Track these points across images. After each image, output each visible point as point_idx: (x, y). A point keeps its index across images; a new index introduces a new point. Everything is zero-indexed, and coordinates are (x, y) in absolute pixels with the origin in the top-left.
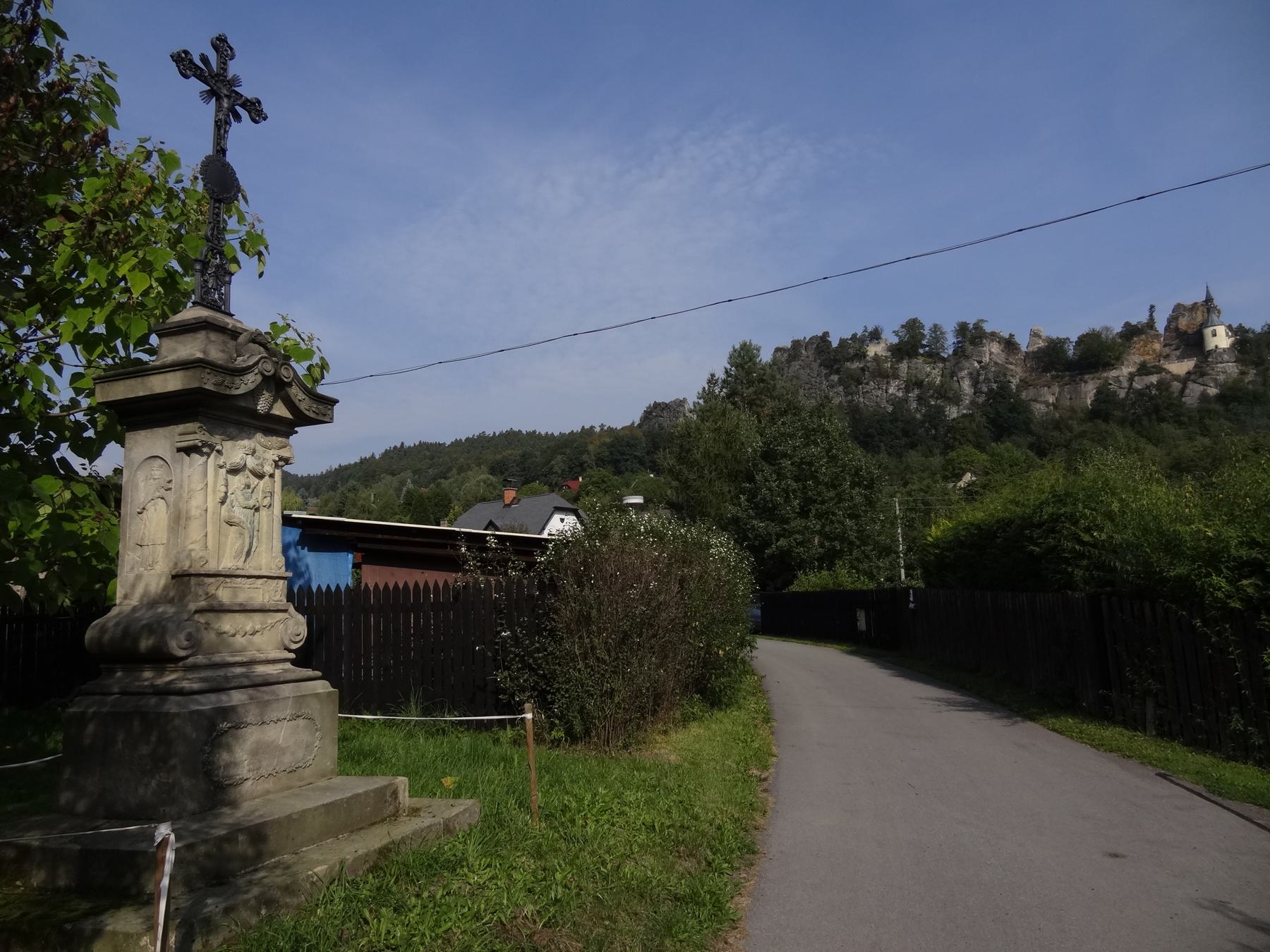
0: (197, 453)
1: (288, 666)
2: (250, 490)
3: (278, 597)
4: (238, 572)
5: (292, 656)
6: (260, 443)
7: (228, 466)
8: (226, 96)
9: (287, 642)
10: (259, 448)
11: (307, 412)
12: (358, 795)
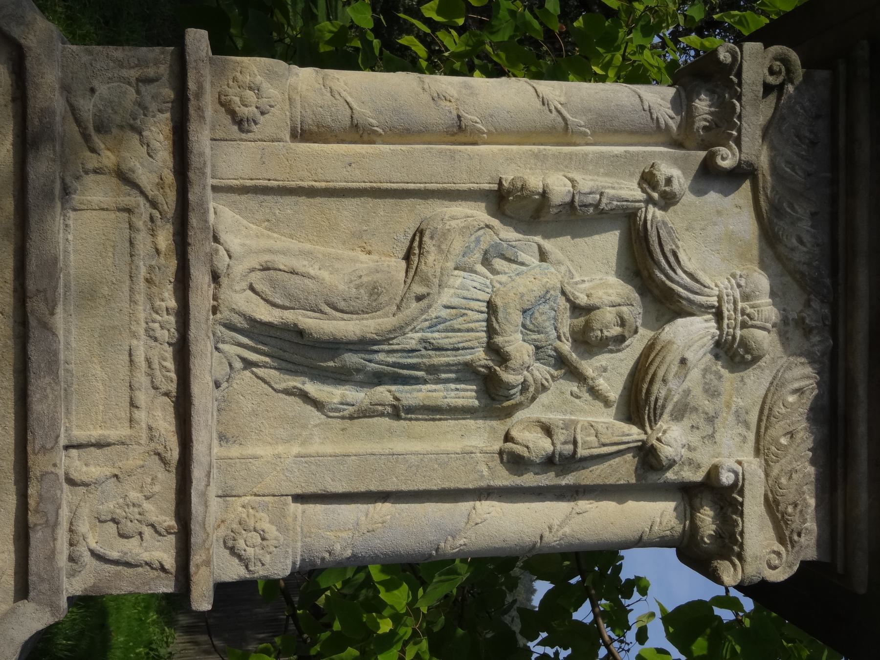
6: (775, 385)
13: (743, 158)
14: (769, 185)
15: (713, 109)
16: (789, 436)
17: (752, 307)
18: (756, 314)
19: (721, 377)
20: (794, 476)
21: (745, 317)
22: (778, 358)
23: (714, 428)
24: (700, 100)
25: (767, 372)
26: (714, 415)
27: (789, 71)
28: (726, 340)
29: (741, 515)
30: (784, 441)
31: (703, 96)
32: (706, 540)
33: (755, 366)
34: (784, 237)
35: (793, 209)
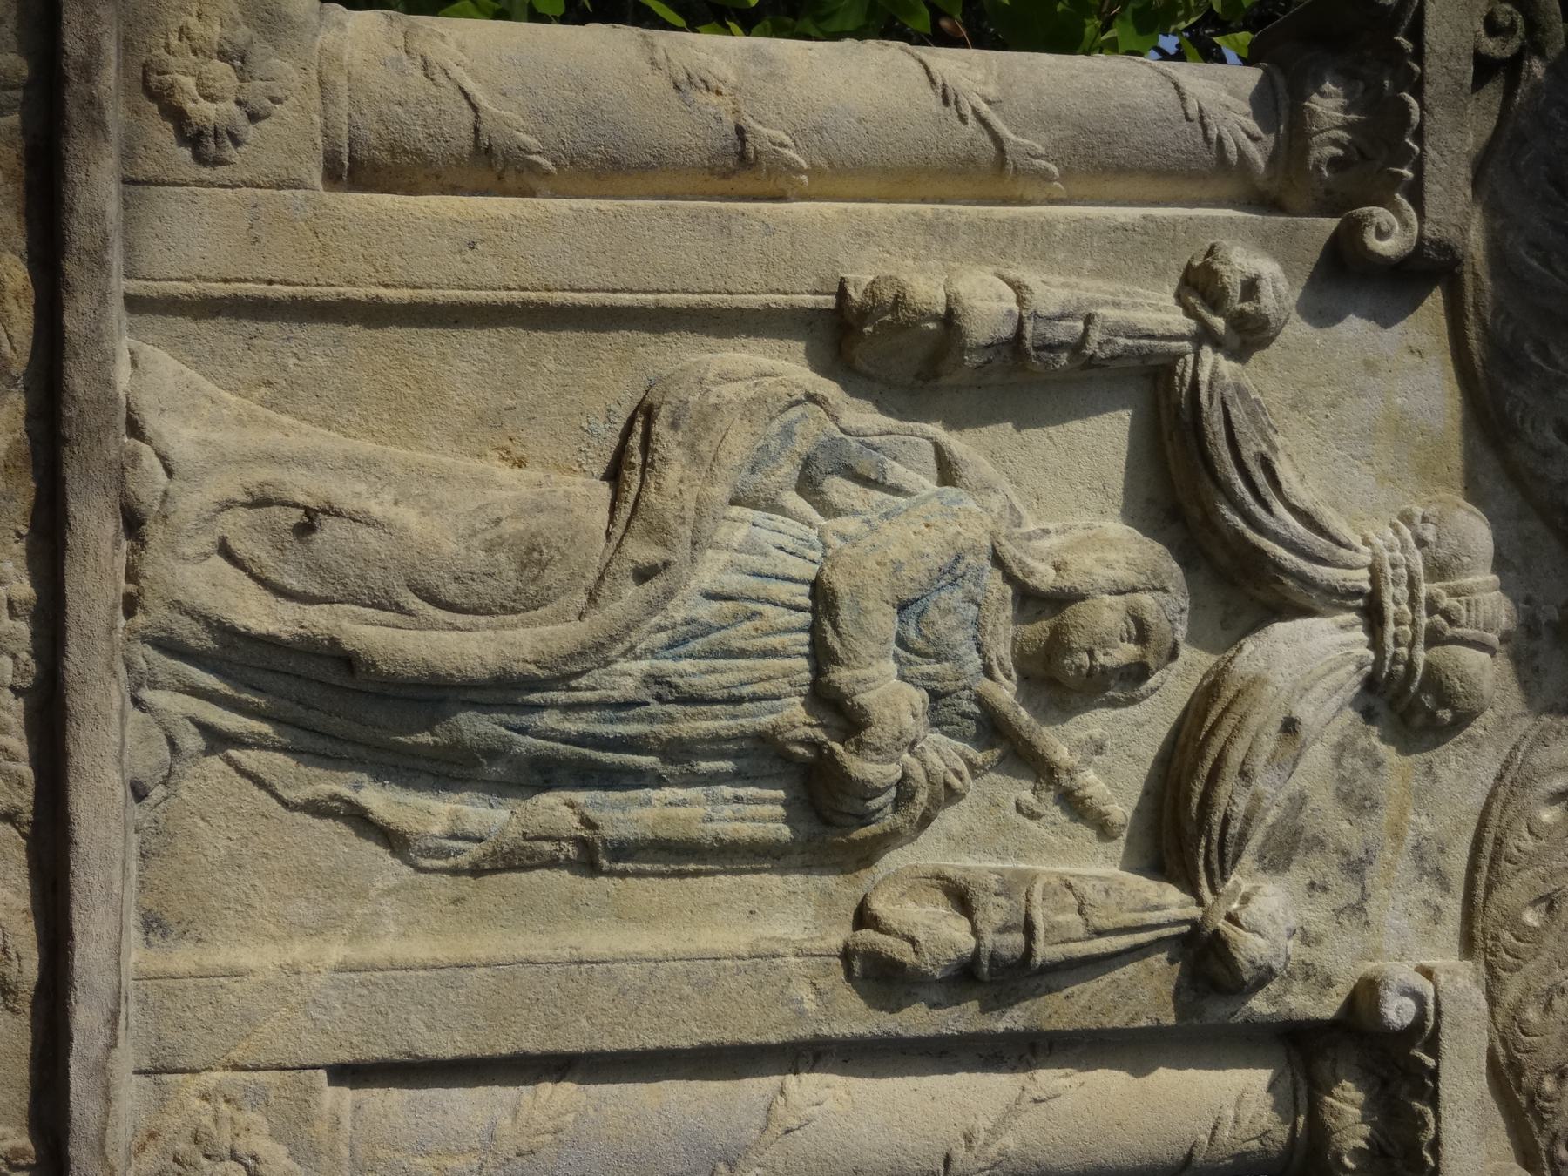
2: (1004, 693)
13: (1428, 234)
14: (1487, 299)
15: (1353, 117)
16: (1544, 905)
17: (1454, 593)
18: (1464, 611)
19: (1378, 764)
20: (1558, 1002)
21: (1437, 617)
22: (1514, 716)
23: (1363, 888)
24: (1322, 95)
25: (1489, 750)
26: (1363, 856)
27: (1532, 26)
28: (1390, 675)
29: (1434, 1100)
30: (1531, 918)
31: (1328, 86)
32: (1347, 1161)
33: (1461, 737)
34: (1527, 425)
35: (1547, 357)
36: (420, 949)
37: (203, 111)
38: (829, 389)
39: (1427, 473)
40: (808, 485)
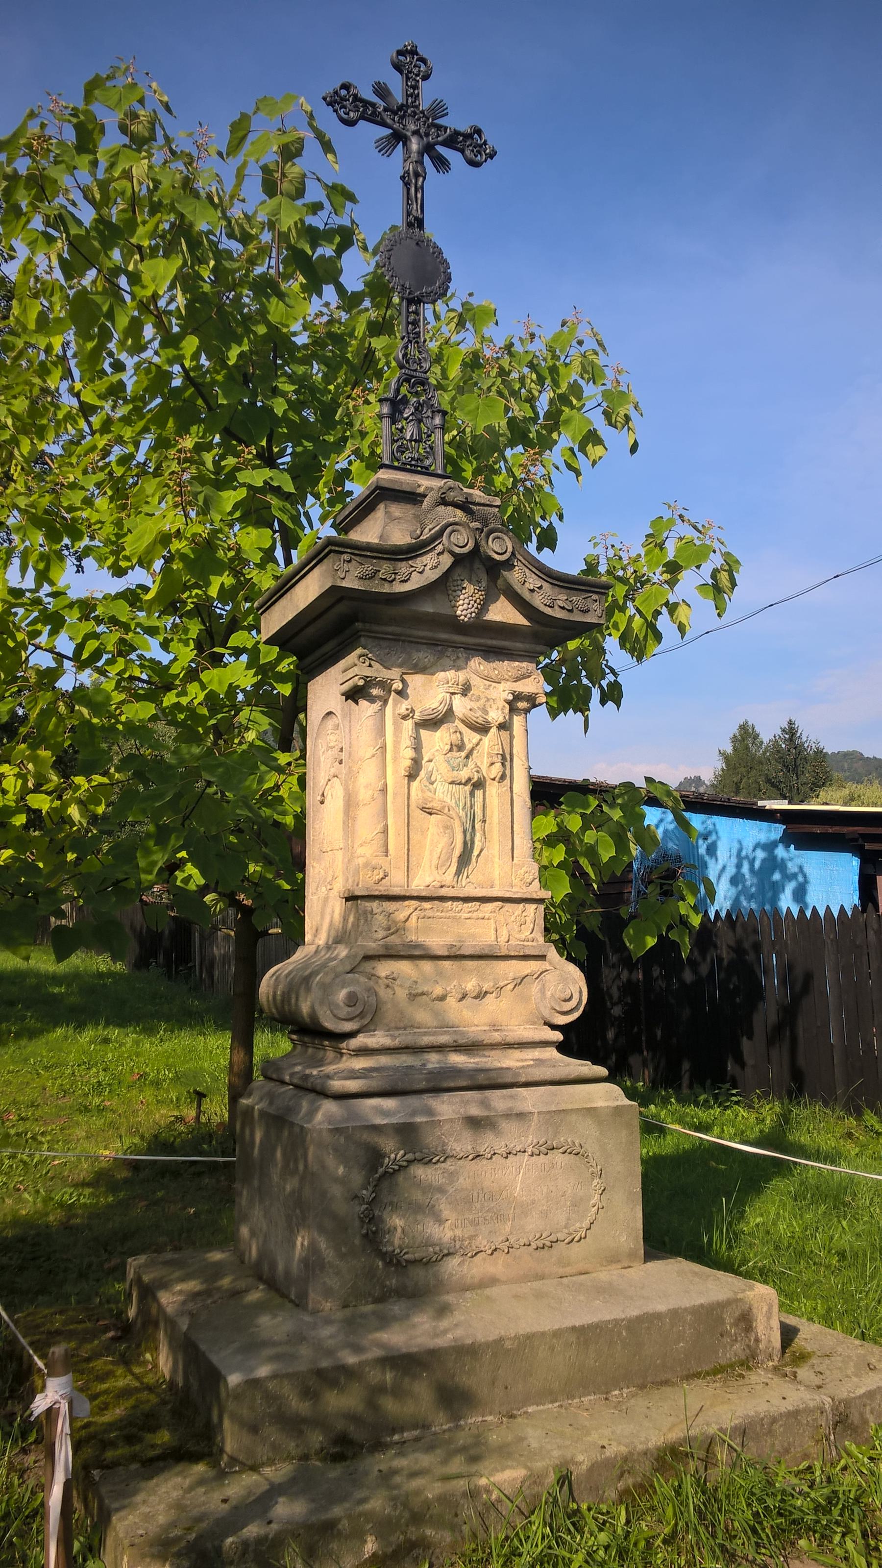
0: (364, 698)
1: (553, 1053)
2: (463, 754)
3: (526, 933)
4: (443, 892)
5: (558, 1036)
6: (477, 673)
7: (417, 716)
8: (416, 133)
9: (546, 1013)
10: (475, 681)
11: (548, 611)
12: (658, 1316)
36: (496, 847)
37: (381, 875)
38: (418, 779)
39: (431, 681)
40: (432, 783)
